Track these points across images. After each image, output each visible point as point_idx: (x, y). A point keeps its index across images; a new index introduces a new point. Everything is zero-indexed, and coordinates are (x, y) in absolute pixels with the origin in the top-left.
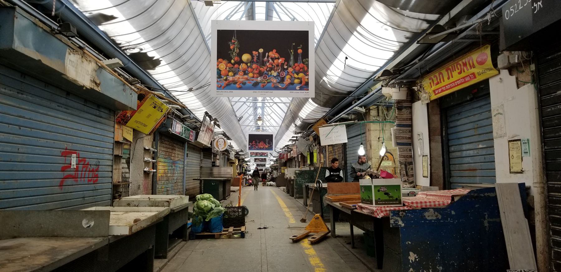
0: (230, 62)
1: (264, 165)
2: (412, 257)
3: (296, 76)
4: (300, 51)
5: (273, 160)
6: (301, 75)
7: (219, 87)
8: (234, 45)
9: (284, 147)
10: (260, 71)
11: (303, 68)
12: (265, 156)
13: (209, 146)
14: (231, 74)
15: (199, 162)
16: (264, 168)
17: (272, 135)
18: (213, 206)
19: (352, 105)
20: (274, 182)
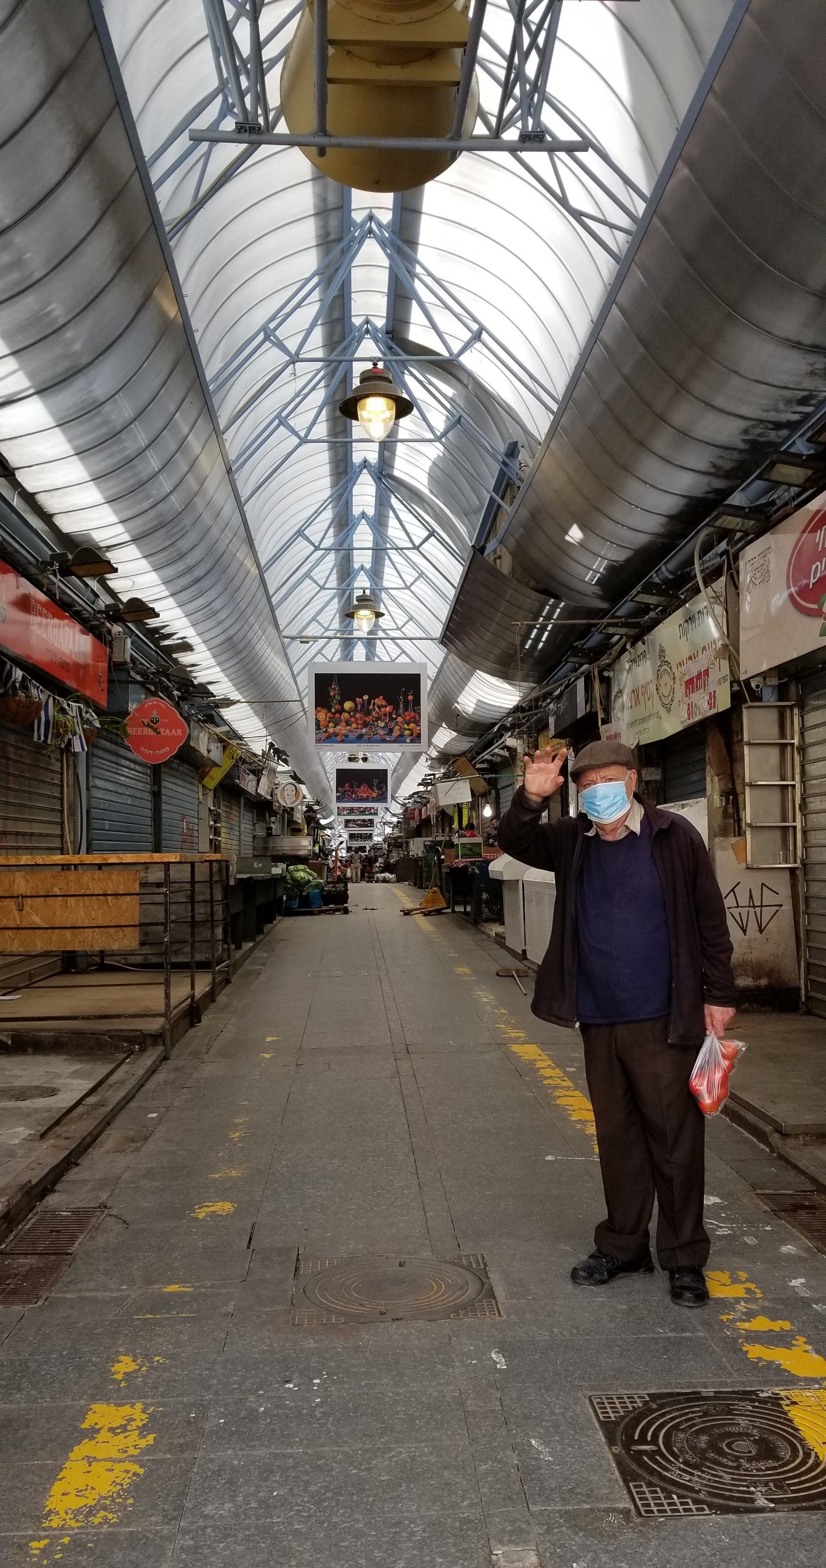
0: (330, 711)
1: (370, 837)
2: (485, 896)
3: (406, 726)
4: (410, 698)
5: (391, 823)
6: (412, 725)
7: (318, 741)
8: (334, 691)
9: (411, 796)
10: (365, 721)
11: (414, 717)
12: (371, 814)
13: (269, 798)
14: (331, 725)
15: (251, 827)
16: (368, 845)
17: (385, 772)
18: (311, 878)
19: (493, 744)
20: (391, 873)
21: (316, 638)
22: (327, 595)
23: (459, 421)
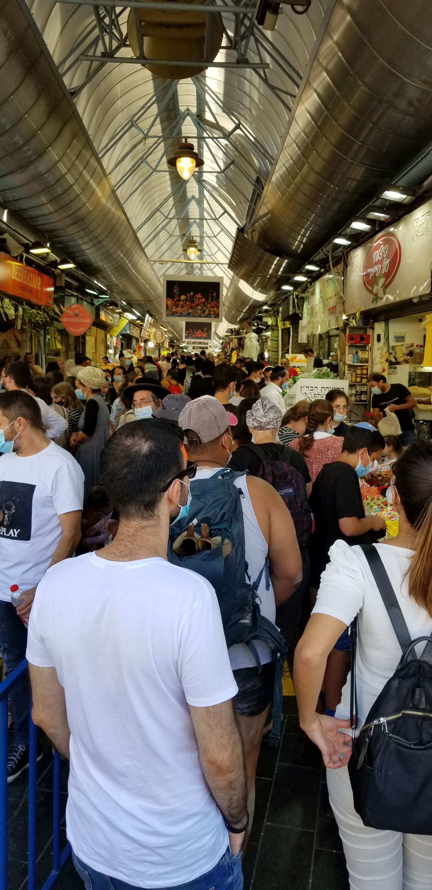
3: (212, 309)
4: (215, 294)
6: (215, 309)
7: (167, 315)
8: (176, 290)
11: (216, 305)
21: (167, 262)
22: (173, 239)
23: (233, 162)
